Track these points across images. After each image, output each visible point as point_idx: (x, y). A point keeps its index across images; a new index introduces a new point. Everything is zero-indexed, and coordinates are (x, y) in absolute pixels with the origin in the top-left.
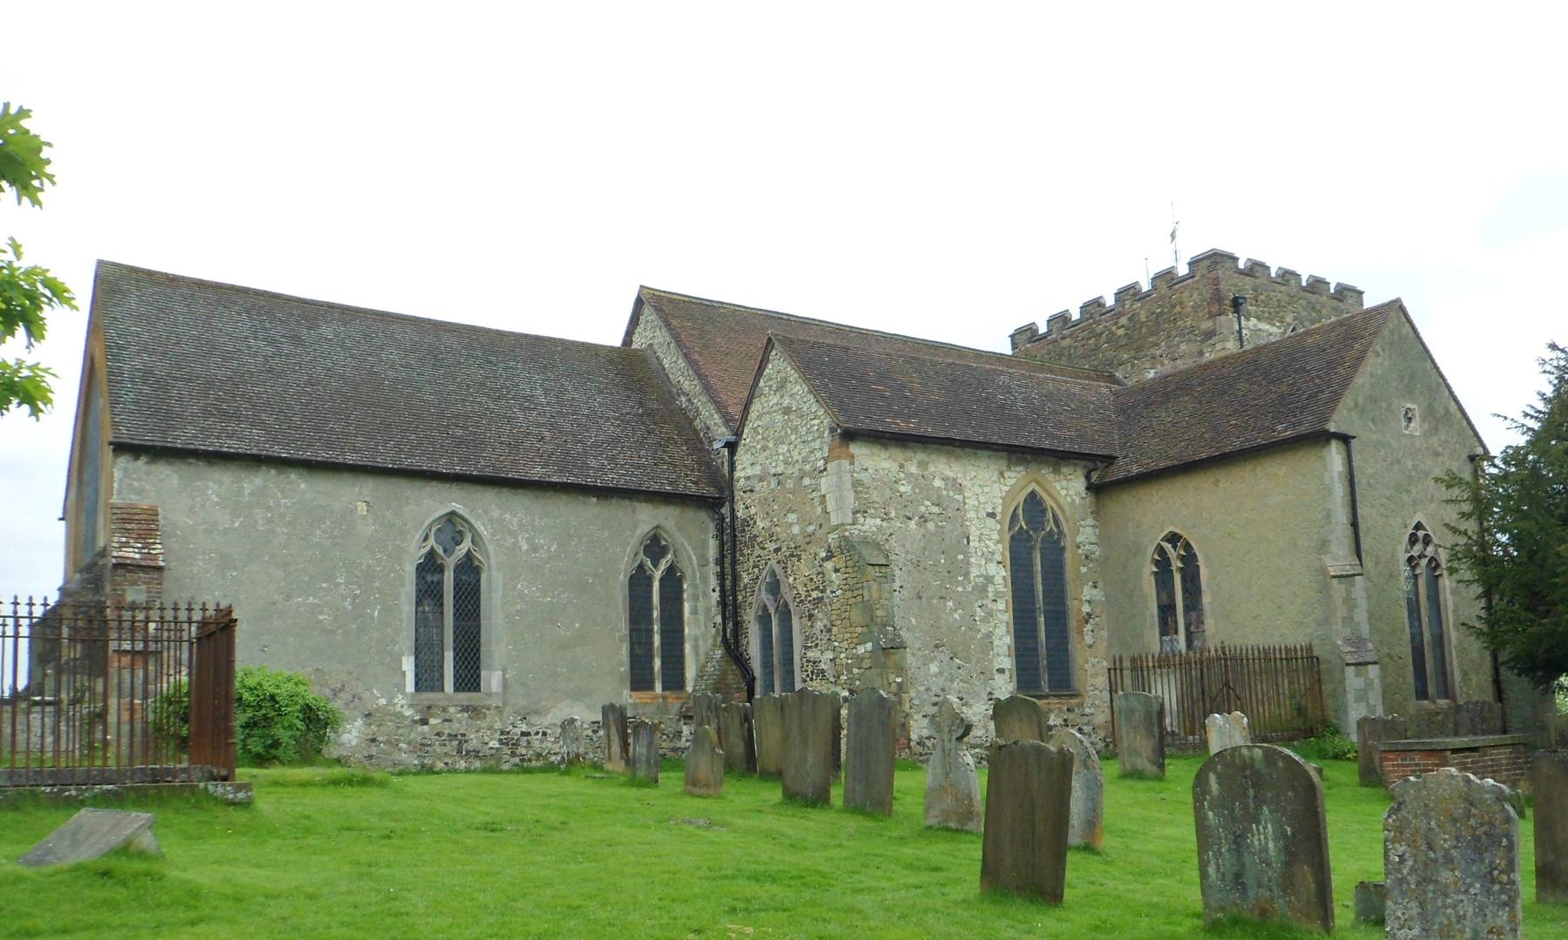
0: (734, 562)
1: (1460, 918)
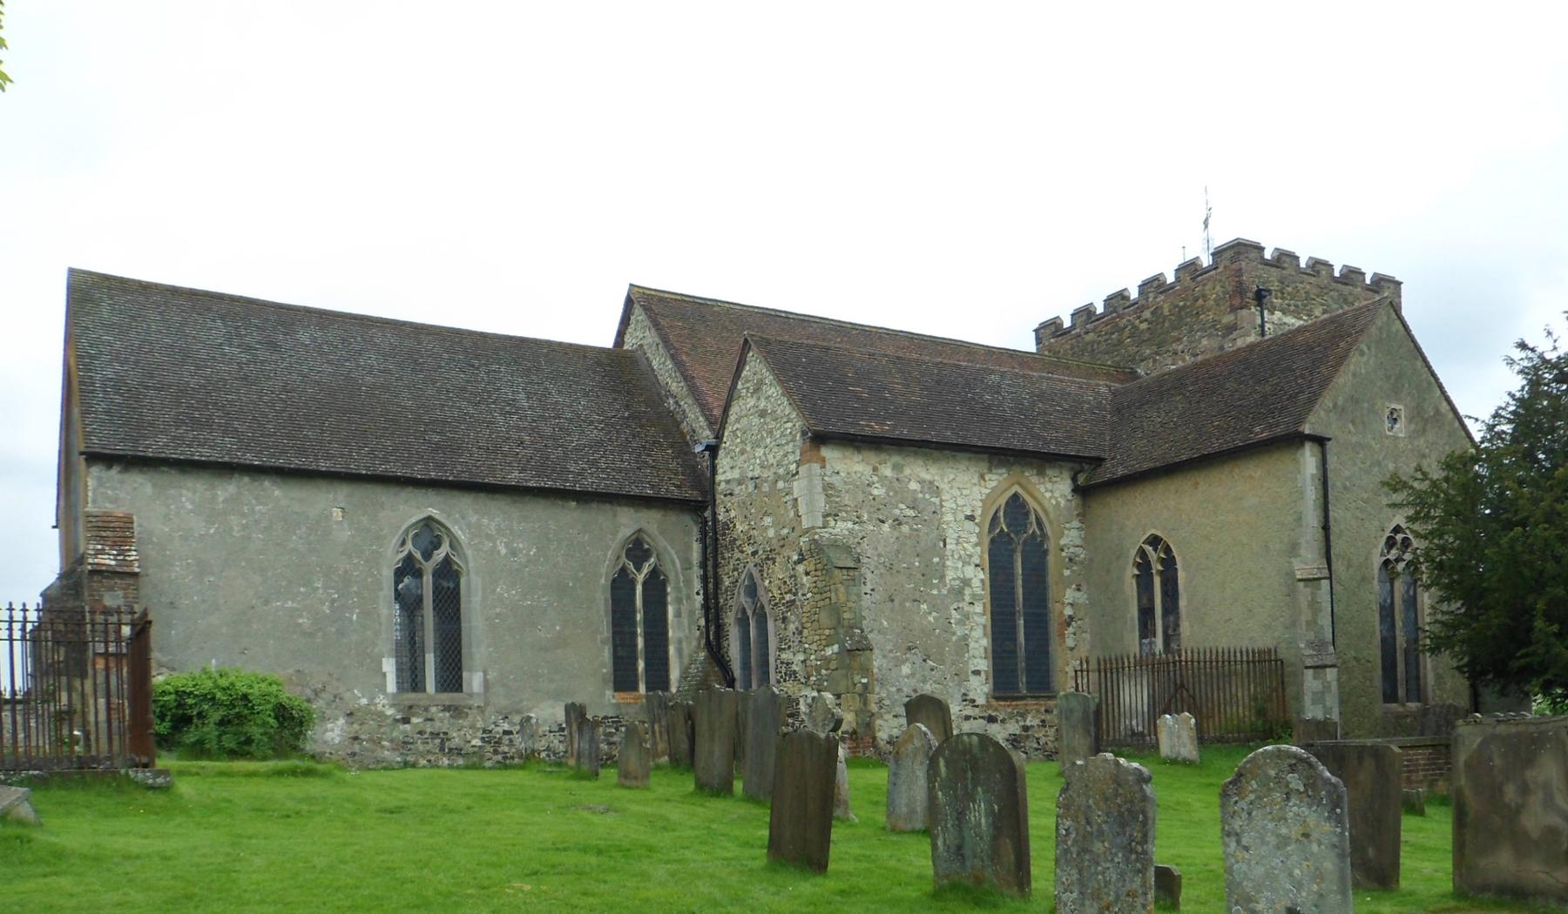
0: (716, 566)
1: (1107, 883)
